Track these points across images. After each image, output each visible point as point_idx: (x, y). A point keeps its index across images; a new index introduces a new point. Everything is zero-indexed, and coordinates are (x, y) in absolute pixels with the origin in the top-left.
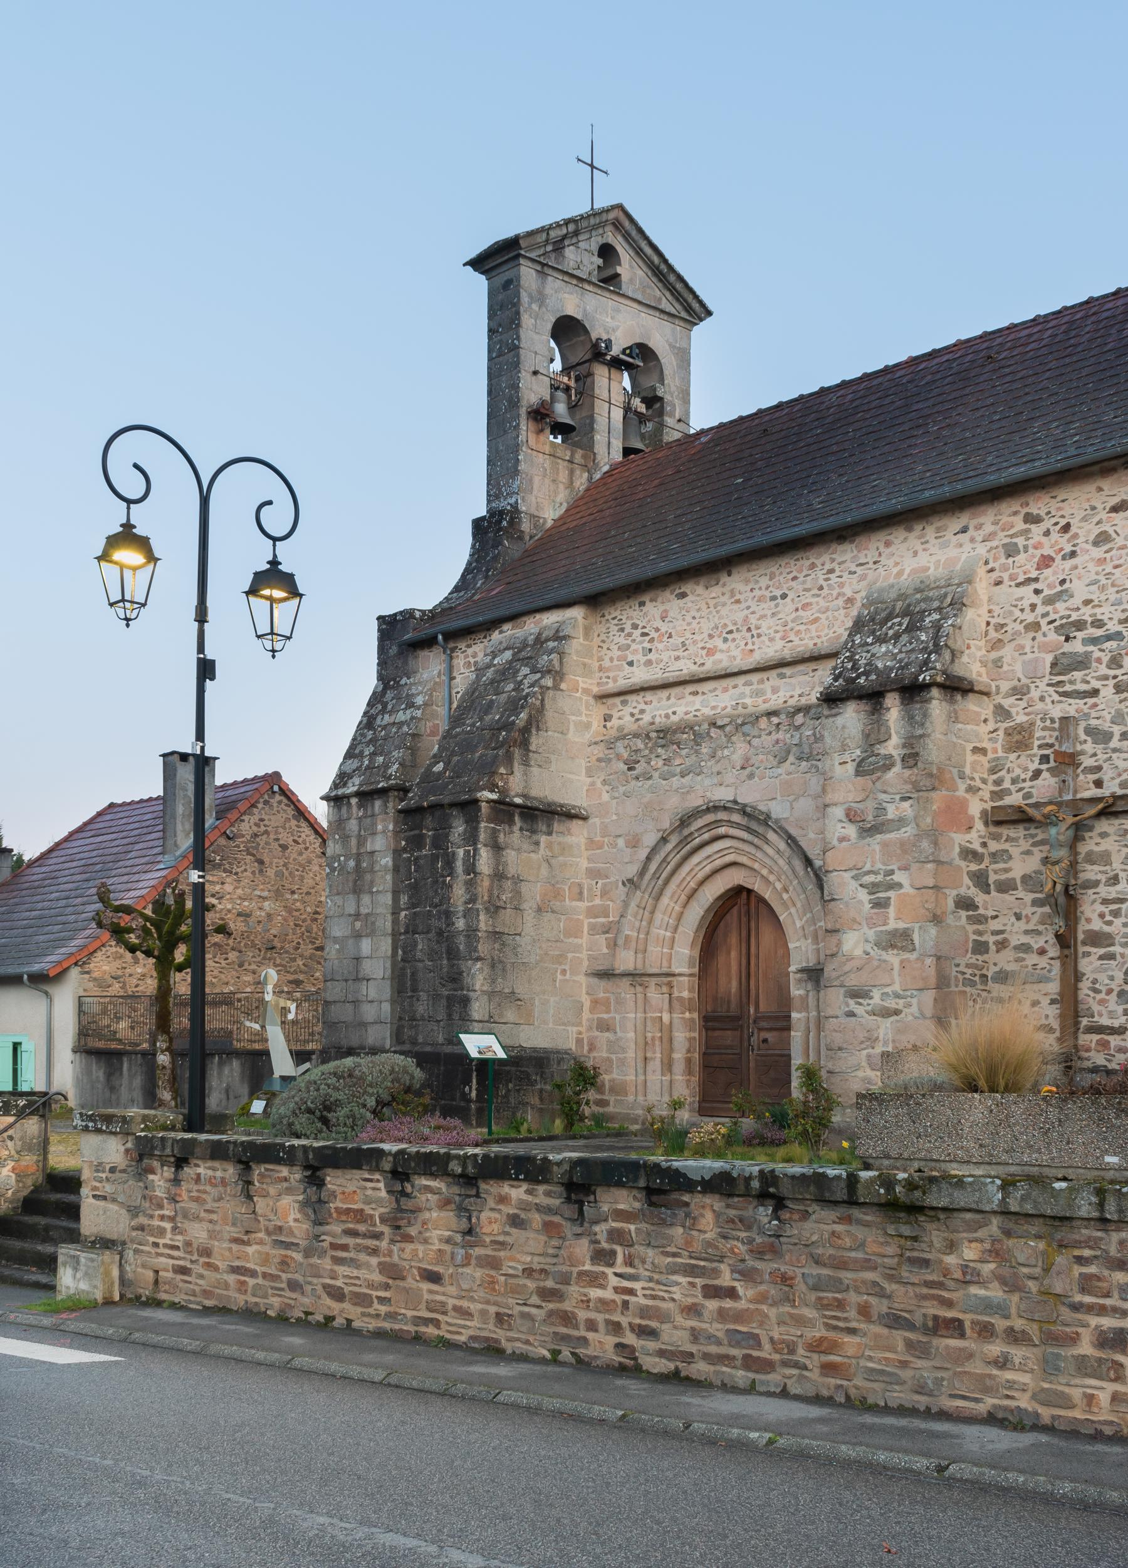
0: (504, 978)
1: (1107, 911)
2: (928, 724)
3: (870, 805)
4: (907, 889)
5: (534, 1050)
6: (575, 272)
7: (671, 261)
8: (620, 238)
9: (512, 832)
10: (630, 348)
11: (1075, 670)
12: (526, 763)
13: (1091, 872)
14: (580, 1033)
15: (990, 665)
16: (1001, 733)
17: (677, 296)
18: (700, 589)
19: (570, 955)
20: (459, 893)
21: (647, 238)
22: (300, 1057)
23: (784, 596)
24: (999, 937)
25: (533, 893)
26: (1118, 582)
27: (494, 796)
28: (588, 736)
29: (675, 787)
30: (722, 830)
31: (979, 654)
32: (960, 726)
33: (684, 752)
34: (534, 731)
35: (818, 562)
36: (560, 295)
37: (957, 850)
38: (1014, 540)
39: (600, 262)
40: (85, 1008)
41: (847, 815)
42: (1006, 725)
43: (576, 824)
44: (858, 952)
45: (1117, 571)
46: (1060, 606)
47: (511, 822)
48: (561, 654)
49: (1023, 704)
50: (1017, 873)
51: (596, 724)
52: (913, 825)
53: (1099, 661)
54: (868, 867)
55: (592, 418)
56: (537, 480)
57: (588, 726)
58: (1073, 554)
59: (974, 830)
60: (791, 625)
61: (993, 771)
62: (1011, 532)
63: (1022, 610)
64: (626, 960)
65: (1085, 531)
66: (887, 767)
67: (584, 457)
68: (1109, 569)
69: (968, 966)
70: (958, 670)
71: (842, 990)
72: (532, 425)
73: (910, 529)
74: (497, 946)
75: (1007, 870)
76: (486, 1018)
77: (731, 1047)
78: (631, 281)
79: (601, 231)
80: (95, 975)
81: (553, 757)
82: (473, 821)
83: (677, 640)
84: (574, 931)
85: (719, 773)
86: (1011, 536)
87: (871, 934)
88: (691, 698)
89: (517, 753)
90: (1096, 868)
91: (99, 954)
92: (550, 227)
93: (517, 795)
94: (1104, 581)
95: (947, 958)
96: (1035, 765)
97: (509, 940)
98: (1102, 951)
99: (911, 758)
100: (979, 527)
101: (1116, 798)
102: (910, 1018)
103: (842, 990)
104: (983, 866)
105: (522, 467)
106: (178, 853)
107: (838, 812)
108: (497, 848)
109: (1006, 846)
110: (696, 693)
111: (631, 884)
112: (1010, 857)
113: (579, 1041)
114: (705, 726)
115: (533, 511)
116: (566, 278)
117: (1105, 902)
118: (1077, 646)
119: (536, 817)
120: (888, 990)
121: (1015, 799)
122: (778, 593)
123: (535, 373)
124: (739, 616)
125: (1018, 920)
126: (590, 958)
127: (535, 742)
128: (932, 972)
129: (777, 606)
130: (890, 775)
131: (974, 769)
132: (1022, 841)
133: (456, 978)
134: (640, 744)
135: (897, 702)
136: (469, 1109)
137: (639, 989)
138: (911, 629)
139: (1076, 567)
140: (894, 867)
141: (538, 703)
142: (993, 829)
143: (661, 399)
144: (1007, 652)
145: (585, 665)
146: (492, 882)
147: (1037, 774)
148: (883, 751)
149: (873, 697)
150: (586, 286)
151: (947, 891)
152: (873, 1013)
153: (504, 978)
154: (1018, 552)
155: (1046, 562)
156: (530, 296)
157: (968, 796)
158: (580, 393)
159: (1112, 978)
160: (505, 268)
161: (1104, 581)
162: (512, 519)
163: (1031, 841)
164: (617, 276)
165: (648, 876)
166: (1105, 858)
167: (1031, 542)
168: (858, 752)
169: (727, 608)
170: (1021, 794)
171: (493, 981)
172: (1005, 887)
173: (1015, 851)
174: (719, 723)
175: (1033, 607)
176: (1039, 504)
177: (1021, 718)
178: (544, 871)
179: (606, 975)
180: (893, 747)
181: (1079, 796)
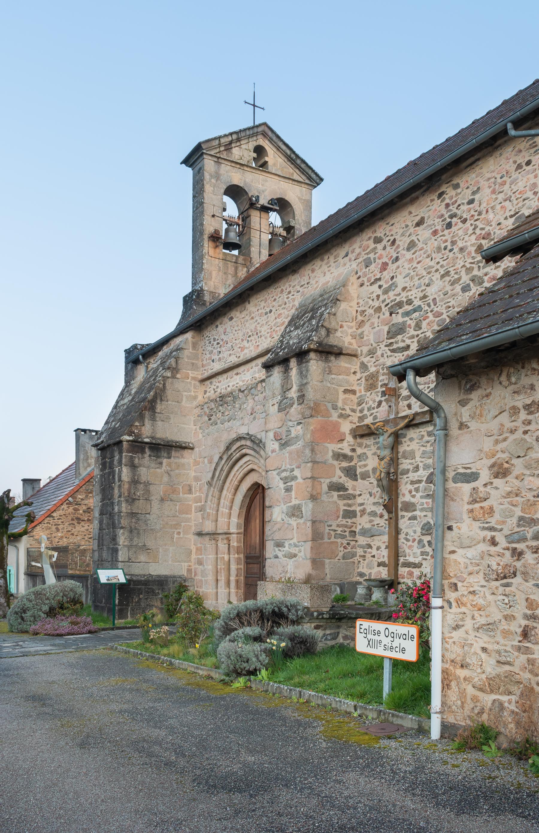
0: (138, 537)
1: (413, 488)
2: (309, 376)
3: (284, 429)
4: (300, 480)
5: (159, 576)
6: (238, 161)
7: (297, 152)
8: (267, 142)
9: (144, 458)
10: (271, 200)
11: (399, 334)
12: (153, 419)
13: (405, 464)
14: (190, 566)
15: (358, 337)
16: (363, 379)
17: (303, 171)
18: (238, 314)
19: (183, 524)
20: (116, 491)
21: (282, 140)
22: (58, 577)
23: (271, 311)
24: (362, 508)
25: (158, 491)
26: (419, 273)
27: (131, 438)
28: (195, 403)
29: (226, 427)
30: (244, 451)
31: (350, 331)
32: (333, 376)
33: (229, 408)
34: (158, 401)
35: (284, 288)
36: (230, 174)
37: (331, 454)
38: (369, 256)
39: (255, 155)
40: (31, 554)
41: (275, 436)
42: (366, 374)
43: (186, 452)
44: (279, 519)
45: (419, 266)
46: (391, 294)
47: (143, 452)
48: (177, 359)
49: (374, 360)
50: (369, 468)
51: (200, 398)
52: (302, 440)
53: (410, 326)
54: (283, 468)
55: (249, 239)
56: (214, 274)
57: (195, 398)
58: (397, 259)
59: (345, 441)
60: (274, 328)
61: (359, 404)
62: (367, 251)
63: (373, 300)
64: (209, 527)
65: (403, 242)
66: (292, 405)
67: (244, 260)
68: (415, 265)
69: (338, 526)
70: (333, 340)
71: (272, 542)
72: (211, 244)
73: (322, 260)
74: (133, 520)
75: (365, 466)
76: (127, 560)
77: (256, 574)
78: (274, 165)
79: (255, 138)
80: (36, 537)
81: (172, 416)
82: (121, 453)
83: (229, 345)
84: (188, 511)
85: (242, 418)
86: (367, 254)
87: (284, 508)
88: (235, 377)
89: (147, 414)
90: (408, 461)
91: (38, 527)
92: (220, 137)
93: (147, 437)
94: (412, 273)
95: (320, 522)
96: (378, 399)
97: (142, 517)
98: (410, 514)
99: (302, 398)
100: (353, 252)
101: (416, 414)
102: (301, 559)
103: (272, 542)
104: (352, 464)
105: (205, 266)
106: (81, 478)
107: (271, 435)
108: (133, 467)
109: (365, 451)
110: (237, 374)
111: (209, 484)
112: (367, 457)
113: (189, 571)
114: (237, 392)
115: (212, 289)
116: (233, 165)
117: (412, 483)
118: (398, 319)
119: (160, 449)
120: (291, 542)
121: (369, 421)
122: (268, 310)
123: (213, 216)
124: (253, 327)
125: (368, 495)
126: (196, 525)
127: (159, 407)
128: (309, 531)
129: (268, 318)
130: (293, 409)
131: (344, 403)
132: (372, 447)
133: (114, 539)
134: (213, 405)
135: (295, 364)
136: (115, 610)
137: (213, 542)
138: (312, 318)
139: (398, 267)
140: (294, 466)
141: (161, 386)
142: (359, 440)
143: (293, 227)
144: (366, 328)
145: (193, 364)
146: (130, 485)
147: (380, 403)
148: (289, 396)
149: (285, 362)
150: (246, 168)
151: (322, 480)
152: (285, 556)
153: (138, 537)
154: (371, 263)
155: (384, 266)
156: (211, 175)
157: (340, 420)
158: (243, 227)
159: (415, 532)
160: (198, 162)
161: (412, 273)
162: (198, 294)
163: (377, 446)
164: (266, 163)
165: (215, 479)
166: (411, 455)
167: (377, 255)
168: (279, 397)
169: (248, 322)
170: (372, 417)
171: (131, 540)
172: (365, 476)
173: (369, 454)
174: (242, 389)
175: (378, 296)
176: (381, 230)
177: (373, 369)
178: (166, 479)
179: (200, 534)
180: (293, 393)
181: (400, 415)
